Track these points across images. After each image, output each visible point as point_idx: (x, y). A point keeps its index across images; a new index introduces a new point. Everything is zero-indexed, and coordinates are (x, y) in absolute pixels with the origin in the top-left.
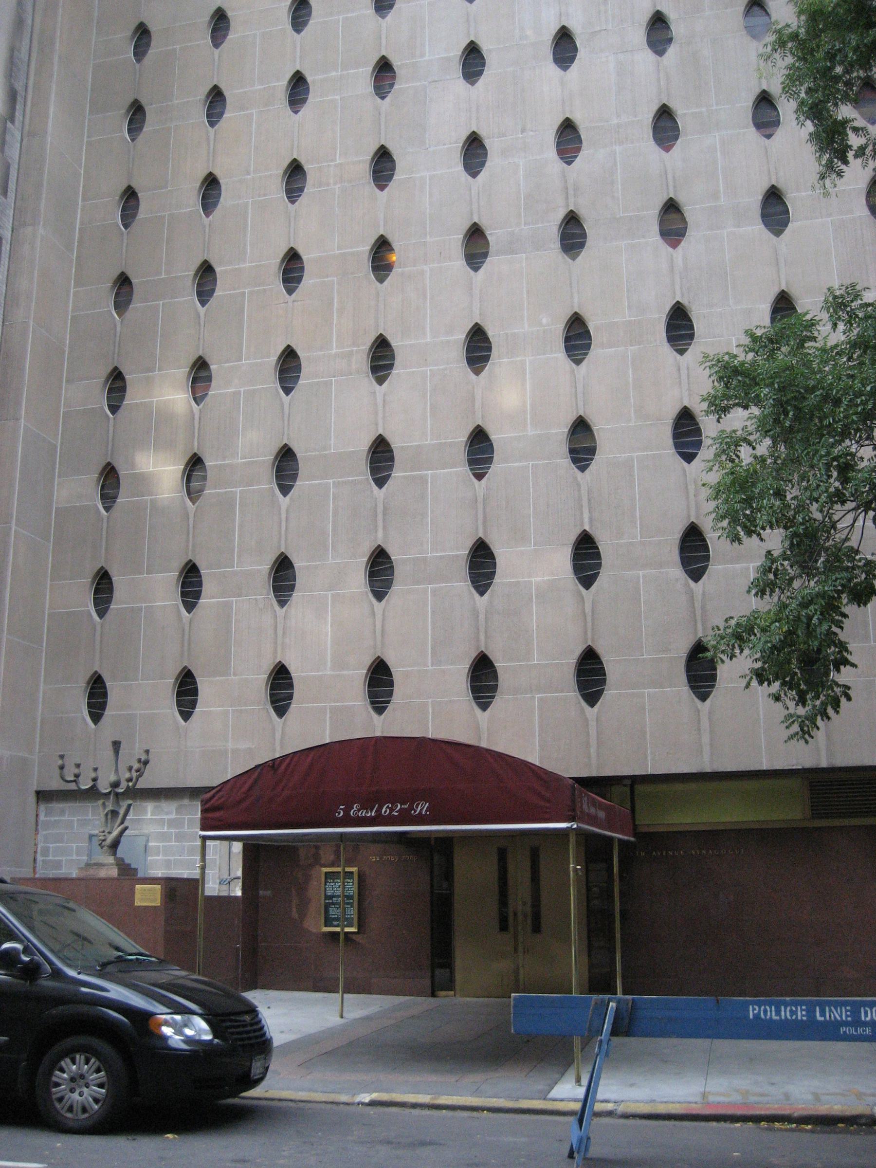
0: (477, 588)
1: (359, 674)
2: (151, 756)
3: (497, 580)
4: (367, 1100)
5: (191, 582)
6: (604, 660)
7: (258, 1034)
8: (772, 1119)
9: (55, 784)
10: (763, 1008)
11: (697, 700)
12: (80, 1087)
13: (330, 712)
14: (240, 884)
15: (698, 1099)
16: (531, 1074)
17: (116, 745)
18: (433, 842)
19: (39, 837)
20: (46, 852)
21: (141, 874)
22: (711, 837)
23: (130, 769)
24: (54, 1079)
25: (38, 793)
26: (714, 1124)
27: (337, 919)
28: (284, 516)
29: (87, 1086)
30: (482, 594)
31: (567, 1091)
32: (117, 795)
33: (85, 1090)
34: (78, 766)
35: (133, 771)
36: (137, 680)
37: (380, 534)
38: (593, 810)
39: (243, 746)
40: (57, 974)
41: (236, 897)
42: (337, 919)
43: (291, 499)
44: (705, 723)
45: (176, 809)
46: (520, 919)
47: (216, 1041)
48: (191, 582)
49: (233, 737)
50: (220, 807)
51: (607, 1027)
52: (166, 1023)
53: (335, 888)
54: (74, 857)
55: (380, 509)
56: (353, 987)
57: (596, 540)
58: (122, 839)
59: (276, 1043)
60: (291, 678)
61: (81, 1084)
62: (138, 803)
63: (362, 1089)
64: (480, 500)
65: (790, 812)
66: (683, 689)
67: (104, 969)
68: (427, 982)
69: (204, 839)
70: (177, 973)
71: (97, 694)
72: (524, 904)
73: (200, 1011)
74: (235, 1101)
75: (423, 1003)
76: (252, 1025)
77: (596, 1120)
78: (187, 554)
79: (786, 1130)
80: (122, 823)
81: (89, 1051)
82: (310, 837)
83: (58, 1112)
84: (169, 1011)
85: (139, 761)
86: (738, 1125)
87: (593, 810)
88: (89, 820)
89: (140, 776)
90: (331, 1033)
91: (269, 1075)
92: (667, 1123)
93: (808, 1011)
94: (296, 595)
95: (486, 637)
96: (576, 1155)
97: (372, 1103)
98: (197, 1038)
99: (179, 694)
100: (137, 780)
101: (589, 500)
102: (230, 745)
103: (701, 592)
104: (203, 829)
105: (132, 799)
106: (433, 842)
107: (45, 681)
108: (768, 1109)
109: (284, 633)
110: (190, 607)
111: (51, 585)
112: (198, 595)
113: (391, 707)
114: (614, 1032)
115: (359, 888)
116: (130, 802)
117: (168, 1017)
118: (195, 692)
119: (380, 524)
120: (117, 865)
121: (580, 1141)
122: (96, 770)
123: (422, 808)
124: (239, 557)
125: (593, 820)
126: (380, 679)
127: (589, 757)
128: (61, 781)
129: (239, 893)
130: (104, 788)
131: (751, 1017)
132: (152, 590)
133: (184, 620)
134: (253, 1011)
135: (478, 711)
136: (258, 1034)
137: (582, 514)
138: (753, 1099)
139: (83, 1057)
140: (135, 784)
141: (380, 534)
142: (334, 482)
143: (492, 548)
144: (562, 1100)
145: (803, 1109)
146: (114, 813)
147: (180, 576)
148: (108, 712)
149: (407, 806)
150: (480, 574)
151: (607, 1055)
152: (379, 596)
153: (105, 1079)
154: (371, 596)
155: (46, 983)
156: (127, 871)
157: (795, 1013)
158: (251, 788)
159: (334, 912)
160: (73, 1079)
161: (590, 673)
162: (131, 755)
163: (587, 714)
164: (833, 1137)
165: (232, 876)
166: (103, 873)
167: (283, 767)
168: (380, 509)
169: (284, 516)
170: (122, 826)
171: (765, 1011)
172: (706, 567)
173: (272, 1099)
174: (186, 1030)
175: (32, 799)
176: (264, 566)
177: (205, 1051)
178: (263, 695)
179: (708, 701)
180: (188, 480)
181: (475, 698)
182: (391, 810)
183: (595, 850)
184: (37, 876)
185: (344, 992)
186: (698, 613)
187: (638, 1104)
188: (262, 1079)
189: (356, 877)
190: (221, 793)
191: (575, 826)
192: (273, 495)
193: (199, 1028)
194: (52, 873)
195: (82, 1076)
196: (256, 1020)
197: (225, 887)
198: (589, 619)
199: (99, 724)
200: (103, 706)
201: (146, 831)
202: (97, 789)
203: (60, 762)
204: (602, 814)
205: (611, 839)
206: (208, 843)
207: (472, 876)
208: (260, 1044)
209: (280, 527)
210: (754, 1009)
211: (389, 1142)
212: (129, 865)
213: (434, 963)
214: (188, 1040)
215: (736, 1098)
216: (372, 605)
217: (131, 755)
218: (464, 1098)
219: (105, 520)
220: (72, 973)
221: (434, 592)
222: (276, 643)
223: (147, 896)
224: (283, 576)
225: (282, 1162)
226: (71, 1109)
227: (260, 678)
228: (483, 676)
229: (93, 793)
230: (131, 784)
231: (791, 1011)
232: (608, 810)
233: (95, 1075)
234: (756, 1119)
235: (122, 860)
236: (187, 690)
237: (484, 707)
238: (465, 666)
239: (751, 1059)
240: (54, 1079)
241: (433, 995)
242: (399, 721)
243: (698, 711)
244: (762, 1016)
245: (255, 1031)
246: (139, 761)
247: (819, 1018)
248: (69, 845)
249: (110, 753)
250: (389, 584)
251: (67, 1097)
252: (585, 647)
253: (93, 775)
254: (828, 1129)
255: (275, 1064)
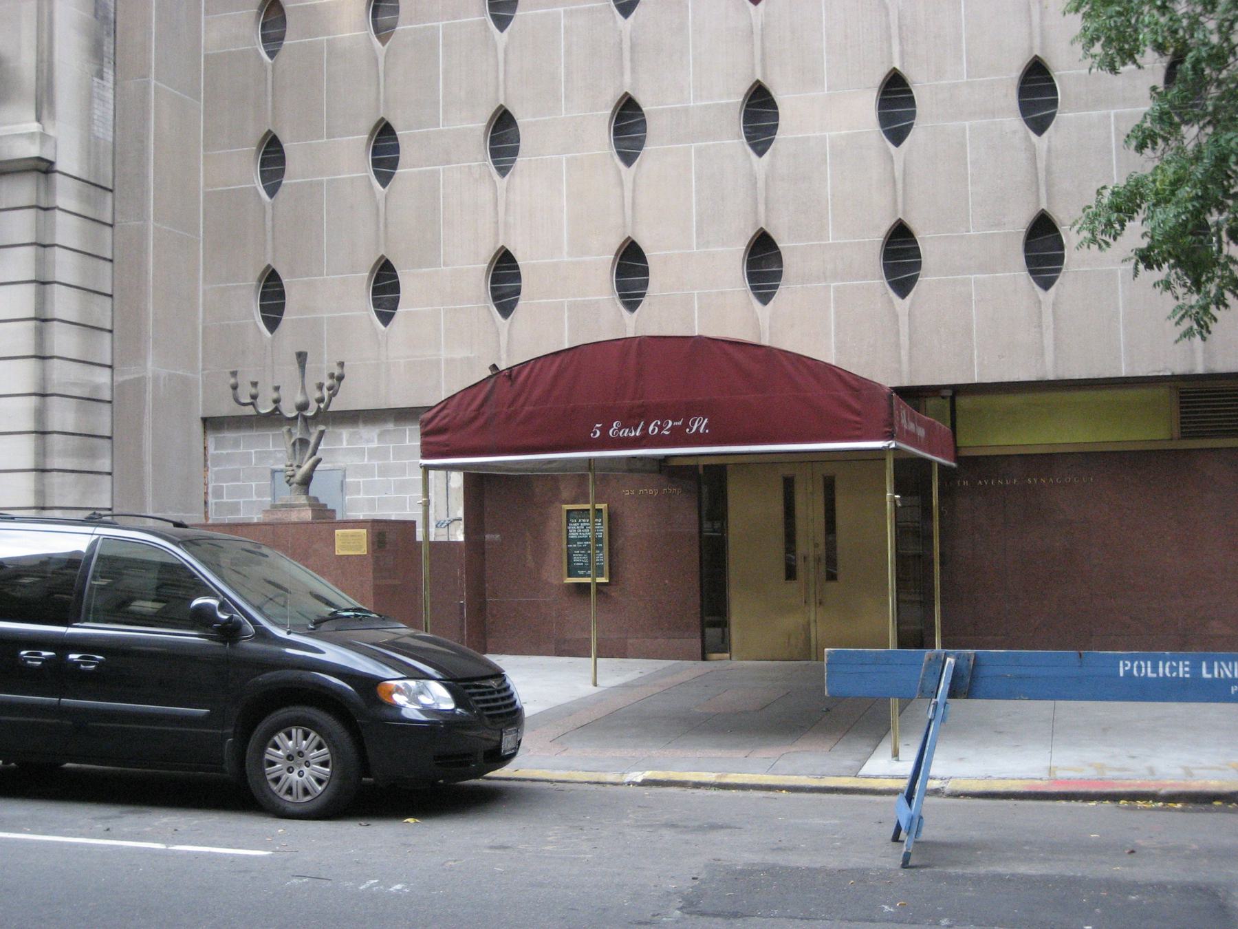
0: (753, 146)
1: (604, 260)
2: (346, 369)
3: (780, 135)
4: (639, 780)
5: (384, 147)
6: (918, 237)
7: (507, 702)
8: (1133, 797)
9: (226, 408)
10: (1136, 663)
11: (1037, 288)
12: (300, 765)
13: (569, 310)
14: (462, 527)
15: (1045, 775)
16: (837, 747)
17: (302, 357)
18: (701, 471)
19: (209, 473)
20: (218, 493)
21: (339, 517)
22: (1043, 462)
23: (320, 387)
24: (267, 757)
25: (205, 420)
26: (1064, 803)
27: (581, 568)
28: (501, 56)
29: (308, 764)
30: (760, 153)
31: (886, 766)
32: (306, 419)
33: (305, 769)
34: (255, 384)
35: (325, 390)
36: (322, 275)
37: (627, 78)
38: (912, 427)
39: (460, 353)
40: (262, 634)
41: (457, 543)
42: (581, 568)
43: (509, 34)
44: (1048, 318)
45: (379, 435)
46: (817, 565)
47: (459, 710)
48: (384, 147)
49: (449, 345)
50: (443, 430)
51: (944, 686)
52: (398, 690)
53: (575, 530)
54: (255, 498)
55: (626, 46)
56: (609, 650)
57: (909, 80)
58: (315, 475)
59: (529, 710)
60: (517, 267)
61: (299, 760)
62: (330, 429)
63: (631, 764)
64: (757, 30)
65: (1152, 429)
66: (1021, 274)
67: (317, 627)
68: (696, 644)
69: (426, 468)
70: (402, 631)
71: (272, 295)
72: (816, 545)
73: (439, 677)
74: (480, 782)
75: (691, 669)
76: (499, 691)
77: (929, 800)
78: (378, 109)
79: (1151, 809)
80: (314, 454)
81: (308, 725)
82: (554, 465)
83: (274, 794)
84: (400, 675)
85: (332, 376)
86: (1093, 804)
87: (912, 427)
88: (270, 453)
89: (334, 395)
90: (584, 703)
91: (520, 752)
92: (1005, 801)
93: (1191, 667)
94: (521, 161)
95: (767, 210)
96: (903, 836)
97: (646, 783)
98: (435, 707)
99: (376, 291)
100: (330, 400)
101: (900, 28)
102: (444, 354)
103: (1045, 147)
104: (424, 456)
105: (326, 424)
106: (701, 471)
107: (205, 280)
108: (1122, 786)
109: (507, 210)
110: (385, 179)
111: (205, 156)
112: (394, 164)
113: (645, 301)
114: (953, 694)
115: (610, 528)
116: (322, 428)
117: (400, 683)
118: (396, 288)
119: (627, 64)
120: (310, 505)
121: (911, 820)
122: (277, 389)
123: (700, 425)
124: (445, 112)
125: (912, 438)
126: (631, 265)
127: (900, 362)
128: (237, 406)
129: (460, 537)
130: (289, 411)
131: (1121, 674)
132: (331, 159)
133: (378, 196)
134: (499, 675)
135: (757, 304)
136: (507, 702)
137: (890, 46)
138: (1109, 774)
139: (300, 731)
140: (328, 405)
141: (627, 78)
142: (565, 11)
143: (773, 94)
144: (877, 777)
145: (1172, 785)
146: (304, 442)
147: (370, 139)
148: (286, 317)
149: (680, 423)
150: (757, 129)
151: (943, 720)
152: (628, 158)
153: (328, 757)
154: (617, 158)
155: (249, 645)
156: (323, 513)
157: (1177, 668)
158: (482, 405)
159: (578, 558)
160: (290, 757)
161: (901, 254)
162: (320, 369)
163: (898, 309)
164: (1209, 817)
165: (452, 517)
166: (294, 516)
167: (522, 378)
168: (626, 46)
169: (501, 56)
170: (314, 458)
171: (1139, 667)
172: (1052, 116)
173: (525, 780)
174: (423, 698)
175: (198, 427)
176: (479, 124)
177: (446, 723)
178: (483, 289)
179: (1053, 290)
180: (375, 15)
181: (753, 288)
182: (661, 428)
183: (912, 476)
184: (210, 522)
185: (599, 655)
186: (1042, 175)
187: (970, 782)
188: (513, 755)
189: (605, 515)
190: (446, 412)
191: (893, 446)
192: (487, 29)
193: (438, 697)
194: (228, 518)
195: (301, 754)
196: (504, 686)
197: (443, 531)
198: (900, 186)
199: (276, 332)
200: (280, 309)
201: (342, 465)
202: (281, 414)
203: (232, 381)
204: (921, 432)
205: (929, 463)
206: (432, 473)
207: (750, 514)
208: (510, 715)
209: (497, 71)
210: (1125, 665)
211: (673, 826)
212: (325, 505)
213: (706, 618)
214: (426, 710)
215: (1090, 773)
216: (619, 172)
217: (320, 369)
218: (758, 776)
219: (270, 68)
220: (281, 633)
221: (699, 152)
222: (497, 222)
223: (351, 543)
224: (503, 133)
225: (548, 848)
226: (290, 791)
227: (477, 270)
228: (763, 260)
229: (274, 418)
230: (322, 406)
231: (1171, 667)
232: (930, 428)
233: (316, 752)
234: (1114, 797)
235: (316, 499)
236: (385, 285)
237: (765, 299)
238: (740, 248)
239: (1104, 730)
240: (267, 757)
241: (704, 659)
242: (657, 318)
243: (1040, 302)
244: (1135, 673)
245: (503, 699)
246: (332, 376)
247: (1205, 675)
248: (248, 483)
249: (294, 367)
250: (640, 143)
251: (284, 778)
252: (894, 221)
253: (275, 396)
254: (1204, 807)
255: (528, 739)
